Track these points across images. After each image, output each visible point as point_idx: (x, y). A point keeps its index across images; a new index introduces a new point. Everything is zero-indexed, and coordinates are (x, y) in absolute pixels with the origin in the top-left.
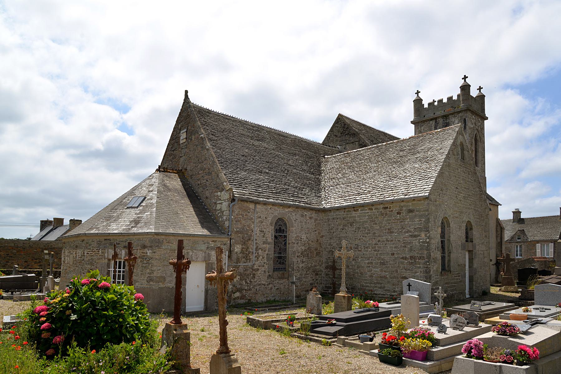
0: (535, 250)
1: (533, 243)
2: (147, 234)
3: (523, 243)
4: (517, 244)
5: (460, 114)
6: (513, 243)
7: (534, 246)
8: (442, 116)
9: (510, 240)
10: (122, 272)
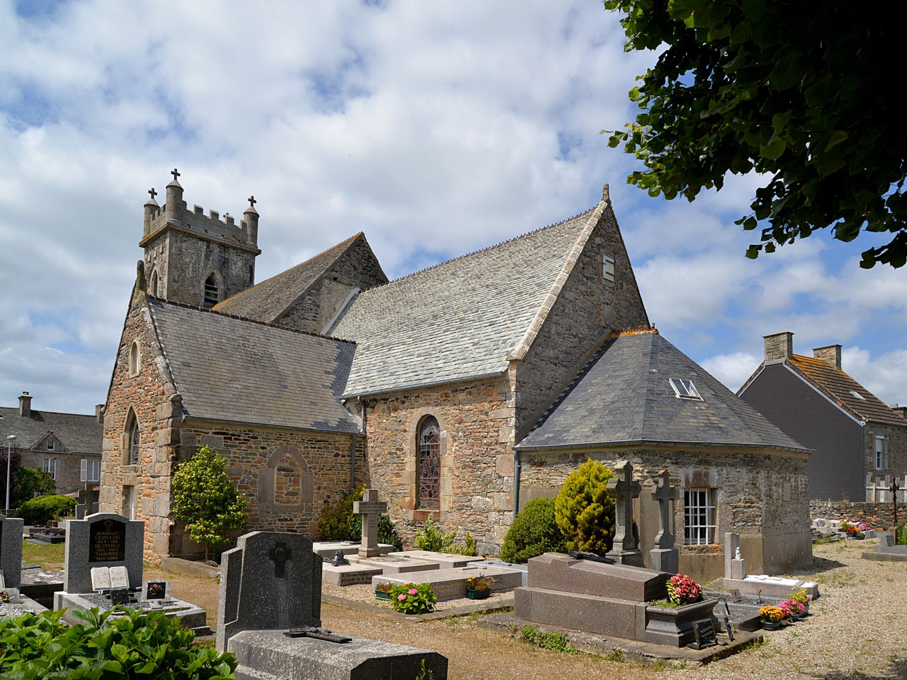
0: (77, 469)
1: (76, 457)
2: (209, 421)
3: (58, 456)
4: (48, 456)
5: (245, 255)
6: (42, 454)
7: (77, 462)
8: (221, 243)
9: (36, 448)
10: (696, 507)
